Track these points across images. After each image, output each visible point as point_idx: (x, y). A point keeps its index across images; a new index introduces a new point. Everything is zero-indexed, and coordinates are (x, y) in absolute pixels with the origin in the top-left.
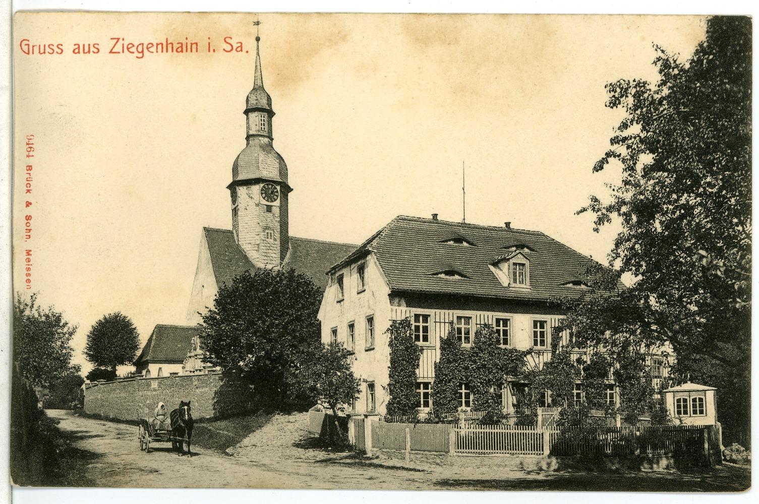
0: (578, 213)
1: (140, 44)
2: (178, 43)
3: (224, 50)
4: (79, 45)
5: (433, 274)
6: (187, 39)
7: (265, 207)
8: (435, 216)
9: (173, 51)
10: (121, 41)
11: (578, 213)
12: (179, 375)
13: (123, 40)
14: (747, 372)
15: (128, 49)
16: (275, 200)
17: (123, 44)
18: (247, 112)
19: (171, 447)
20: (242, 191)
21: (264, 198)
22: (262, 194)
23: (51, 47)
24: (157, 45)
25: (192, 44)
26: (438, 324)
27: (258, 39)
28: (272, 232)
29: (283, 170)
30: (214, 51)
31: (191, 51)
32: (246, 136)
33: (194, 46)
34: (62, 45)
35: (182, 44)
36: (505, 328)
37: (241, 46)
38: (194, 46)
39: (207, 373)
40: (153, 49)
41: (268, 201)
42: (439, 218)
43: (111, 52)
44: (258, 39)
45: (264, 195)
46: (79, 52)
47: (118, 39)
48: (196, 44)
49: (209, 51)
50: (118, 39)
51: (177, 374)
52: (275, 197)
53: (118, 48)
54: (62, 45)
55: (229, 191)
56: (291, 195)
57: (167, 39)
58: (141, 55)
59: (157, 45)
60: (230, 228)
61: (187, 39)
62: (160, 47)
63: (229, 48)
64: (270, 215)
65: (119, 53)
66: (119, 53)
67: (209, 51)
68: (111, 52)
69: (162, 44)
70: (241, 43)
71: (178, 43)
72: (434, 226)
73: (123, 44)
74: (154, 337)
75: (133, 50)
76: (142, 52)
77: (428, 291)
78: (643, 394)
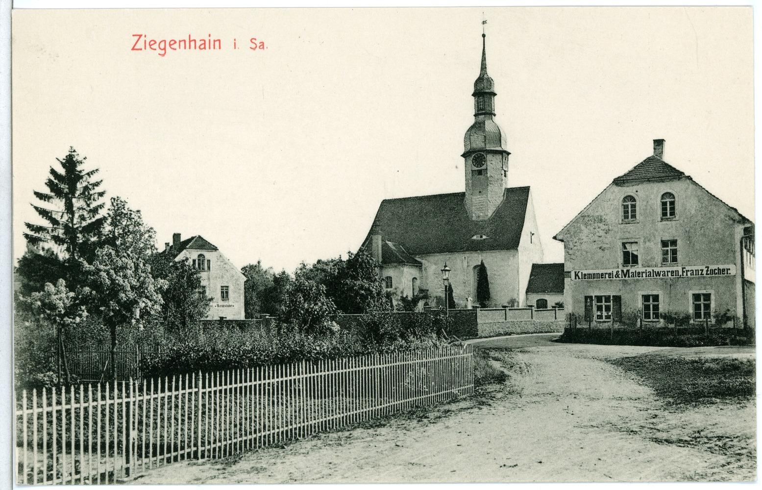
2: (201, 40)
6: (210, 36)
9: (195, 48)
10: (143, 38)
13: (145, 36)
14: (328, 268)
15: (150, 45)
17: (145, 41)
23: (253, 41)
24: (180, 41)
25: (215, 41)
27: (484, 36)
31: (190, 48)
33: (217, 43)
34: (255, 39)
35: (205, 41)
36: (599, 304)
37: (263, 45)
38: (217, 43)
40: (176, 46)
43: (133, 49)
44: (484, 36)
46: (205, 48)
47: (140, 36)
48: (219, 41)
50: (140, 36)
53: (140, 45)
54: (255, 39)
57: (190, 36)
58: (163, 52)
59: (180, 41)
61: (210, 36)
62: (182, 44)
63: (254, 46)
65: (141, 49)
66: (141, 49)
68: (133, 49)
69: (185, 41)
70: (263, 43)
71: (201, 40)
73: (145, 41)
74: (548, 481)
75: (156, 46)
76: (165, 49)
78: (666, 334)
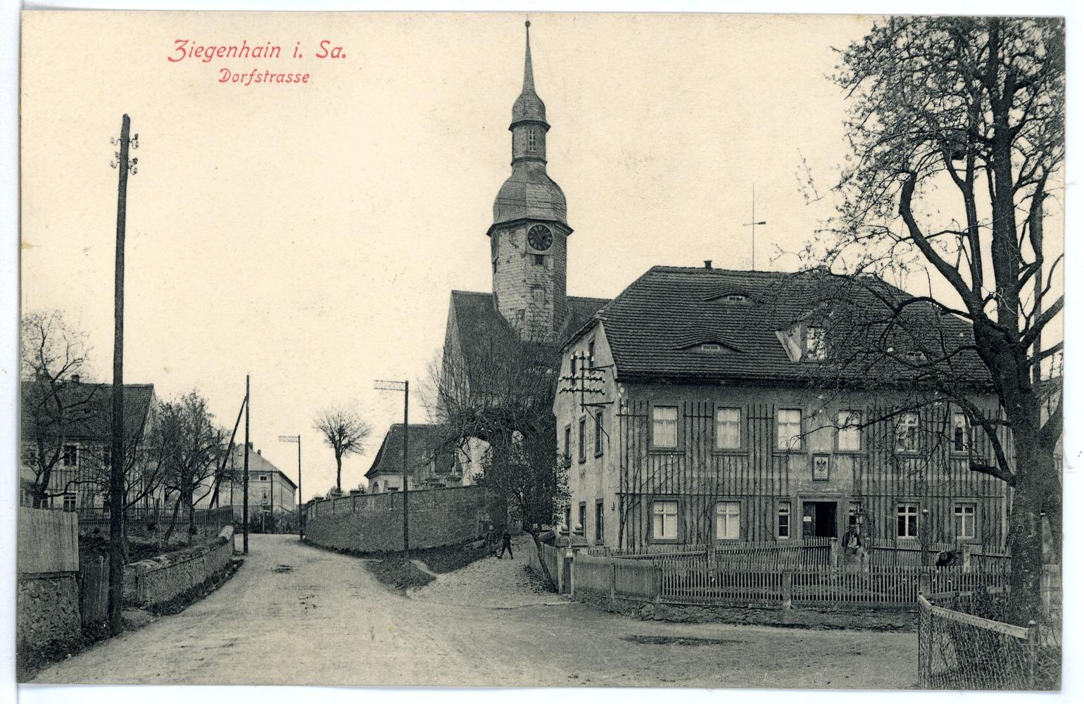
0: (248, 377)
1: (212, 48)
3: (170, 59)
4: (196, 56)
5: (685, 348)
6: (269, 43)
7: (534, 257)
8: (708, 263)
11: (248, 377)
12: (399, 490)
16: (548, 247)
18: (511, 128)
19: (1042, 378)
20: (504, 237)
21: (532, 245)
22: (529, 239)
26: (689, 420)
28: (543, 291)
29: (559, 204)
30: (301, 56)
32: (511, 161)
39: (429, 487)
41: (537, 249)
42: (714, 266)
45: (532, 241)
49: (295, 56)
51: (397, 489)
52: (548, 243)
55: (488, 239)
56: (571, 240)
59: (230, 48)
60: (487, 289)
64: (541, 268)
67: (295, 56)
72: (705, 278)
77: (671, 373)
